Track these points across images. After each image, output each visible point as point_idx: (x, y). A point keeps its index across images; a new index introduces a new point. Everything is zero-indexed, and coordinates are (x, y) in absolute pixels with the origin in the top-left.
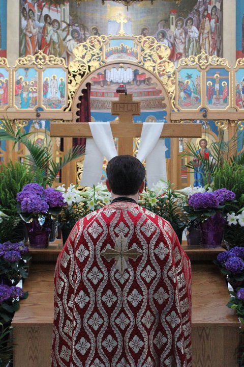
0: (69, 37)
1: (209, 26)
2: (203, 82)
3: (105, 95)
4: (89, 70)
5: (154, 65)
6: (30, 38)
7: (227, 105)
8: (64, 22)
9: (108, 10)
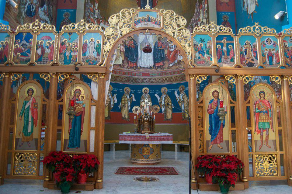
5: (174, 31)
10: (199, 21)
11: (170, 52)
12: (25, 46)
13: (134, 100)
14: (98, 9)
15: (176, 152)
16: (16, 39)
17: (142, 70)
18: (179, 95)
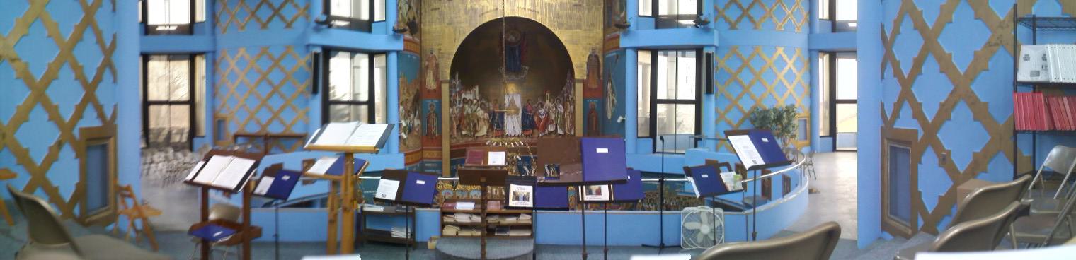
0: (479, 108)
11: (540, 120)
15: (1042, 191)
18: (550, 170)
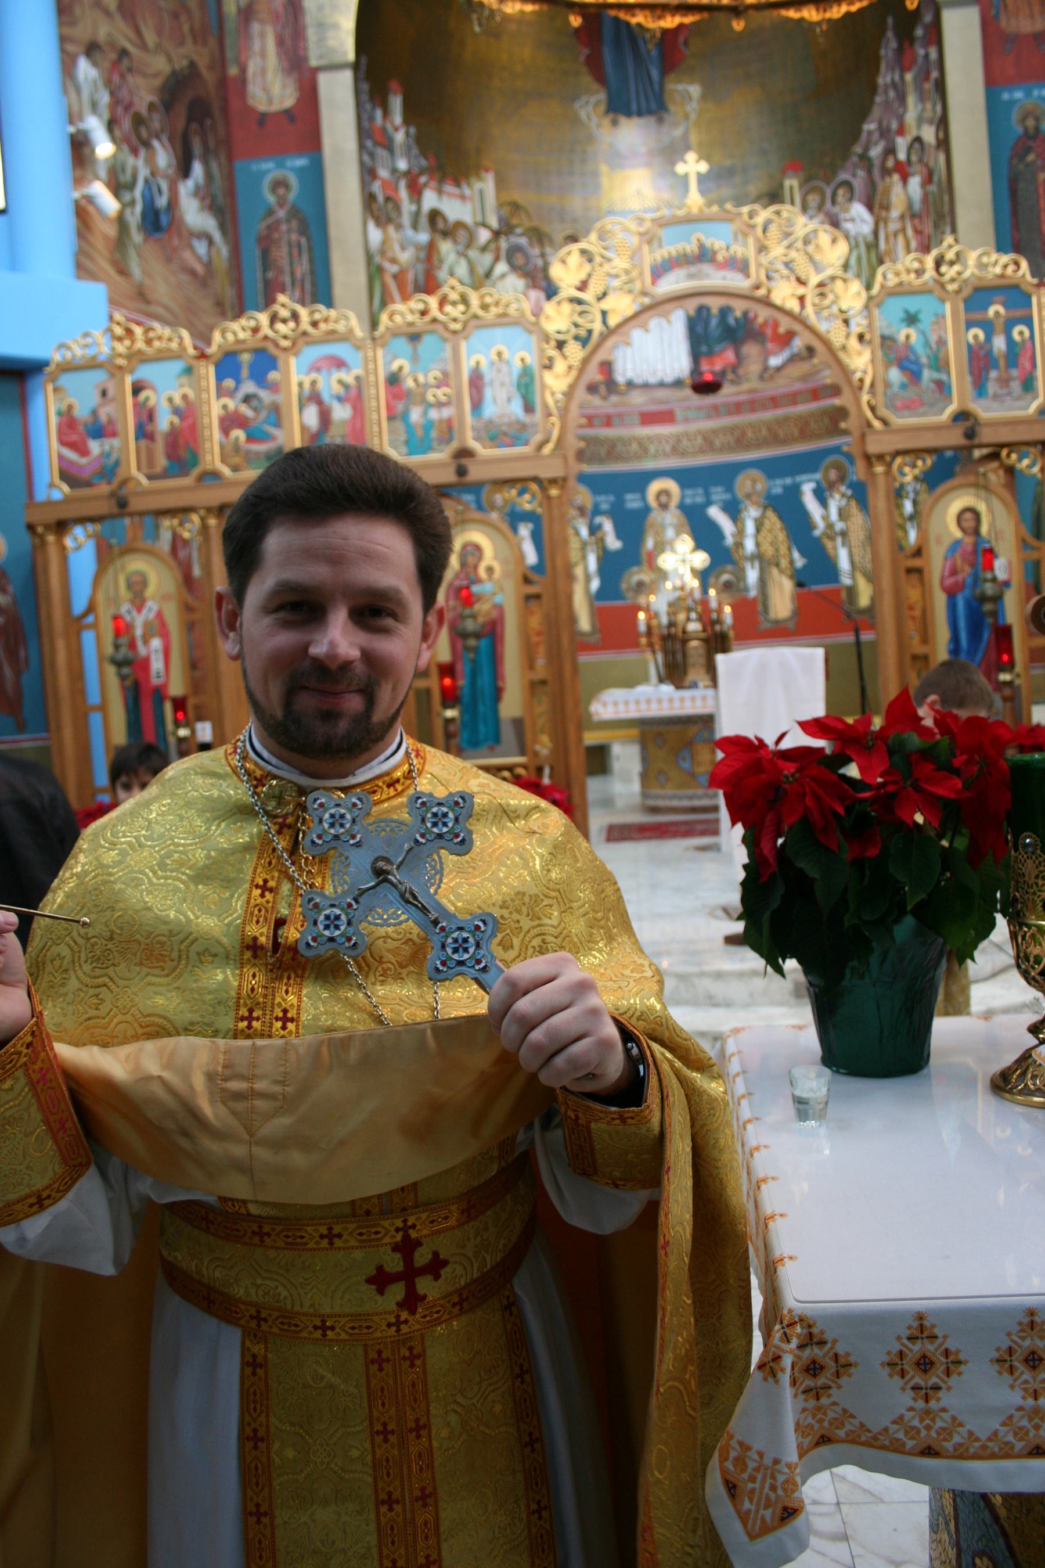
0: (502, 267)
1: (903, 197)
2: (956, 332)
3: (615, 421)
4: (604, 322)
5: (801, 291)
6: (395, 277)
7: (1036, 397)
8: (484, 225)
9: (605, 181)
10: (901, 131)
12: (254, 403)
13: (613, 543)
14: (407, 122)
16: (220, 378)
17: (638, 400)
18: (823, 503)
